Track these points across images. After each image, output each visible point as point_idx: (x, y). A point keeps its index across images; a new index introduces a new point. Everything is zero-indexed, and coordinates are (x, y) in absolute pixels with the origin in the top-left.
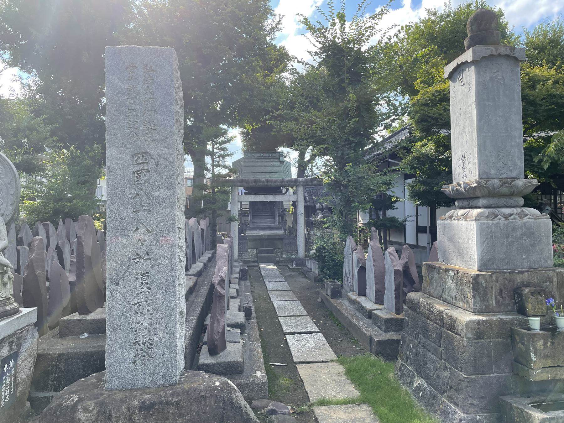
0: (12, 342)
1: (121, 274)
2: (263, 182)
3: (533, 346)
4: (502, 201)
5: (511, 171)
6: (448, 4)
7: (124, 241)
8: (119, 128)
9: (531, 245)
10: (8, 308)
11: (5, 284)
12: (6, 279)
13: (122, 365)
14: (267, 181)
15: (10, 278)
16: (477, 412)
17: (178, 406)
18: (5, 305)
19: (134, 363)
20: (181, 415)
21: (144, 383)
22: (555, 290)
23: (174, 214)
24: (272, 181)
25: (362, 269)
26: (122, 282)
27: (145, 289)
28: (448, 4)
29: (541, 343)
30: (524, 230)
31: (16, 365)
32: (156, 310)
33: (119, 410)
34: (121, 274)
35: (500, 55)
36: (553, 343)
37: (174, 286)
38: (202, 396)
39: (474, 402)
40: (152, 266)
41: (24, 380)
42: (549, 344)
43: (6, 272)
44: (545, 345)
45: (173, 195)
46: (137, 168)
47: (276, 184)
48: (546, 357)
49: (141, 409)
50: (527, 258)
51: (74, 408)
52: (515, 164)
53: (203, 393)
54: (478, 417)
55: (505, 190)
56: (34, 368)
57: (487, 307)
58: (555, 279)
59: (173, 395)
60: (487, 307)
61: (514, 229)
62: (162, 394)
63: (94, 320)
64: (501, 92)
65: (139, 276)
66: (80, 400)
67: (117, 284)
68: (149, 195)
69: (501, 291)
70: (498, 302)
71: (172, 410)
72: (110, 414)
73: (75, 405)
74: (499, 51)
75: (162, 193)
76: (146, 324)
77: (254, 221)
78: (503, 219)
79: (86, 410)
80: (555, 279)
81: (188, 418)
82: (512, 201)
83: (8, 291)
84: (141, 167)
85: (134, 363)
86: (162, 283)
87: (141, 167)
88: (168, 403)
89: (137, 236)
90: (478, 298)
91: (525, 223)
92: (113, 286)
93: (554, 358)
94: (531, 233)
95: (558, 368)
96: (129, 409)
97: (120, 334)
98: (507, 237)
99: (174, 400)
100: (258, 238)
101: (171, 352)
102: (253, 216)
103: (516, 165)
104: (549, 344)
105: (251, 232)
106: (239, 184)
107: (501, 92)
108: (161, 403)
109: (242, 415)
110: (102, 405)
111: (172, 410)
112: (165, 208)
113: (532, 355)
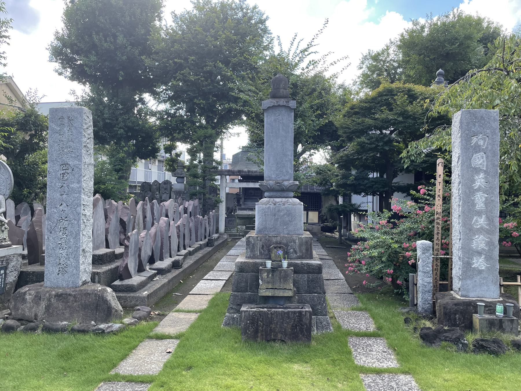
0: (3, 260)
1: (53, 228)
2: (245, 172)
3: (261, 276)
4: (279, 194)
5: (285, 176)
6: (429, 15)
7: (55, 211)
8: (54, 151)
9: (289, 221)
10: (3, 243)
11: (3, 231)
12: (3, 228)
13: (54, 277)
14: (249, 171)
15: (6, 228)
16: (234, 313)
17: (75, 296)
18: (2, 242)
19: (58, 274)
20: (76, 301)
21: (63, 285)
22: (297, 247)
23: (80, 197)
24: (252, 172)
25: (190, 231)
26: (53, 232)
27: (65, 236)
28: (429, 15)
29: (266, 274)
30: (285, 211)
31: (5, 273)
32: (70, 247)
33: (45, 295)
34: (53, 228)
35: (279, 106)
36: (273, 275)
37: (79, 235)
38: (88, 293)
39: (233, 307)
40: (69, 224)
41: (11, 283)
42: (270, 275)
43: (4, 225)
44: (268, 276)
45: (80, 187)
46: (63, 172)
47: (256, 174)
48: (268, 283)
49: (55, 296)
50: (286, 228)
51: (25, 293)
52: (287, 172)
53: (89, 292)
54: (235, 316)
55: (277, 188)
56: (18, 277)
57: (254, 255)
58: (297, 241)
59: (73, 291)
60: (254, 255)
61: (279, 211)
62: (68, 290)
63: (141, 283)
64: (281, 128)
65: (62, 229)
66: (29, 290)
67: (51, 233)
68: (68, 186)
69: (263, 246)
70: (260, 253)
71: (72, 298)
72: (40, 297)
73: (26, 292)
74: (279, 103)
75: (75, 185)
76: (64, 255)
77: (246, 203)
78: (273, 204)
79: (30, 294)
80: (297, 241)
81: (79, 303)
82: (285, 194)
83: (5, 235)
84: (64, 171)
85: (58, 274)
86: (73, 233)
87: (64, 171)
88: (70, 295)
89: (61, 208)
90: (249, 250)
91: (286, 207)
92: (49, 234)
93: (273, 283)
94: (290, 213)
95: (276, 290)
96: (50, 295)
97: (51, 259)
98: (275, 215)
99: (74, 293)
100: (246, 216)
101: (77, 270)
102: (245, 199)
103: (288, 172)
104: (270, 275)
105: (242, 212)
106: (227, 173)
107: (281, 128)
108: (66, 294)
109: (107, 304)
110: (37, 293)
111: (72, 298)
112: (76, 193)
113: (260, 281)
